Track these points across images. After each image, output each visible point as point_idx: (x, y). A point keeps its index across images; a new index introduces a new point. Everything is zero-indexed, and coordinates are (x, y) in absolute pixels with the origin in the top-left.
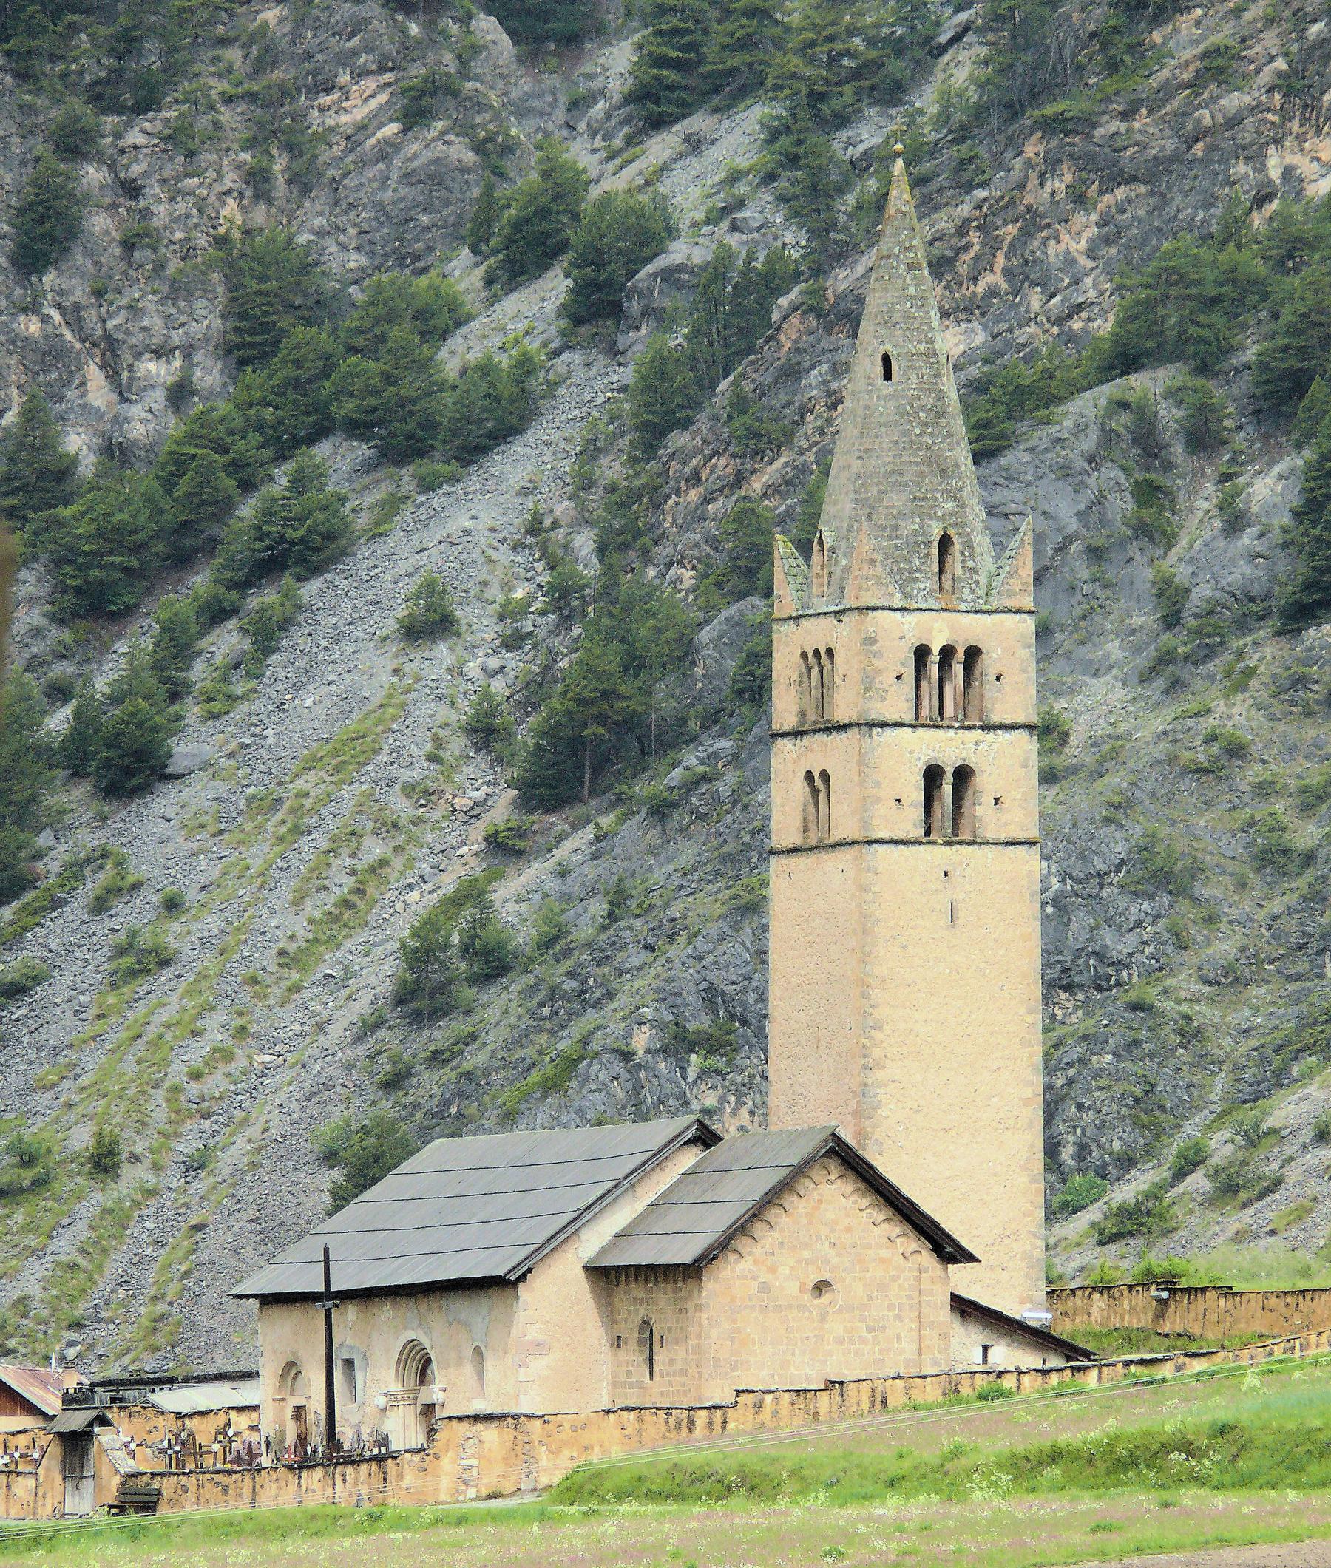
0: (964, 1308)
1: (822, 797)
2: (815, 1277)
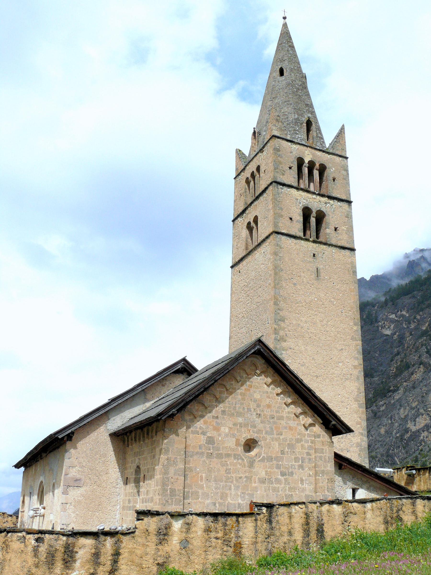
0: (342, 463)
1: (254, 231)
2: (245, 435)
